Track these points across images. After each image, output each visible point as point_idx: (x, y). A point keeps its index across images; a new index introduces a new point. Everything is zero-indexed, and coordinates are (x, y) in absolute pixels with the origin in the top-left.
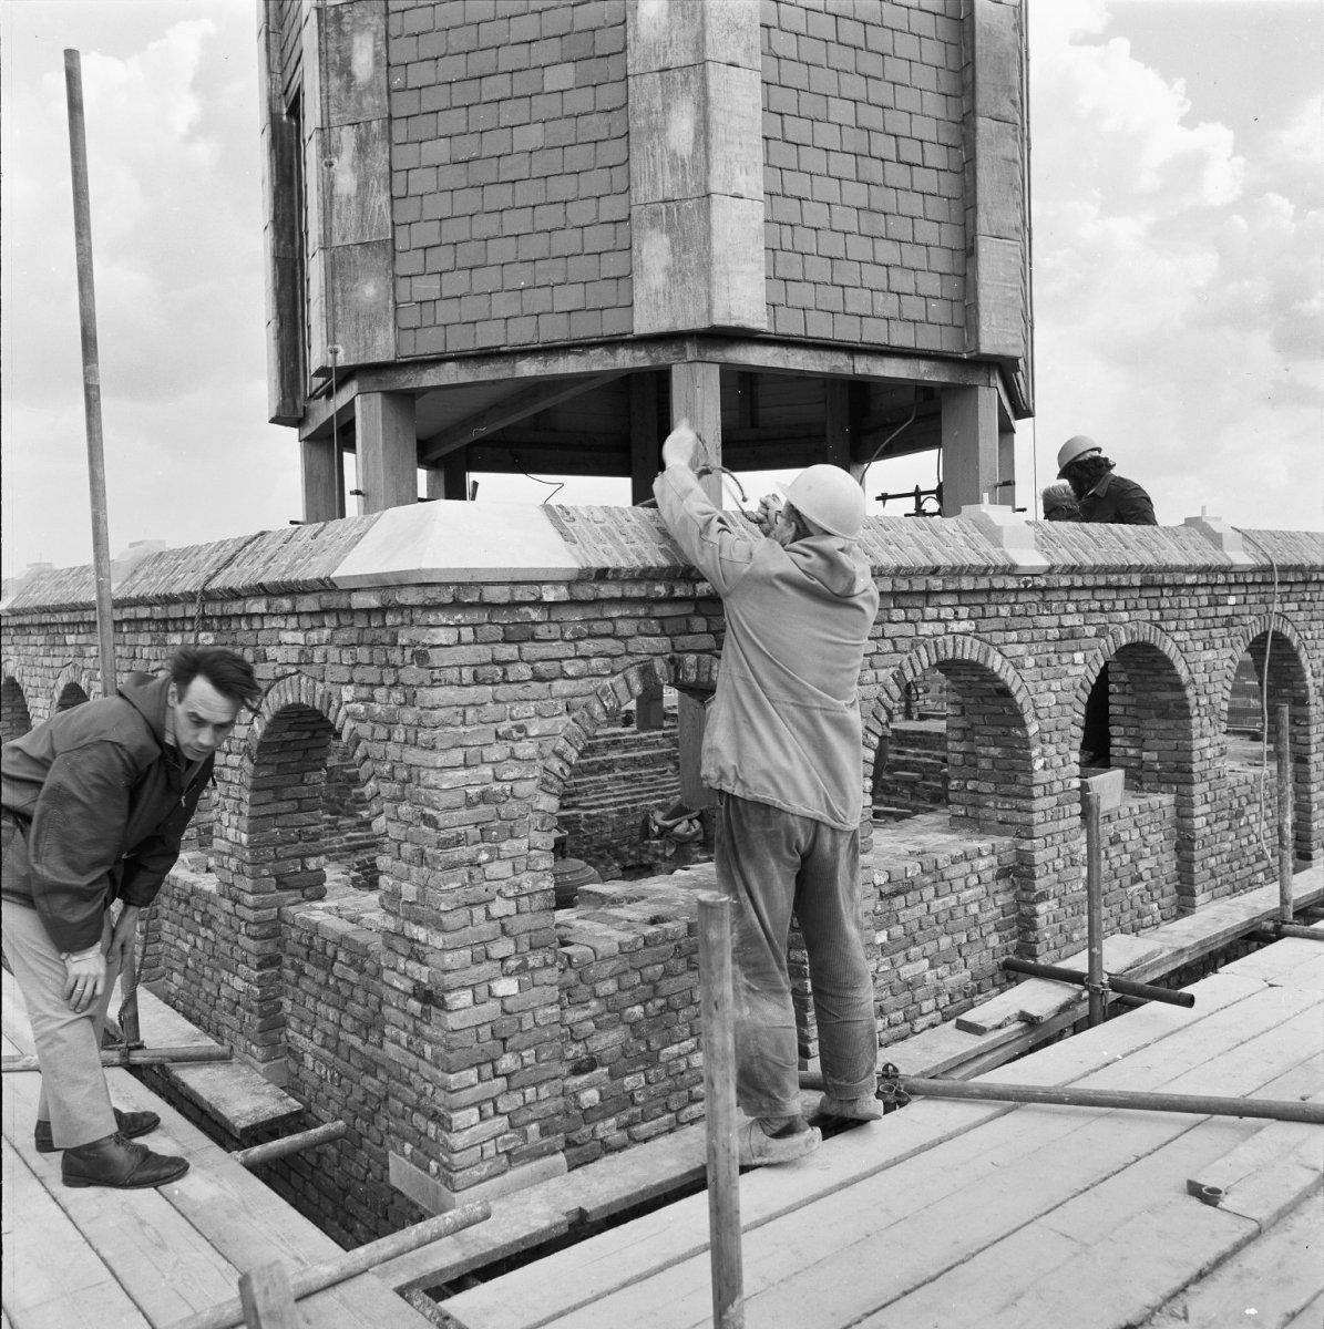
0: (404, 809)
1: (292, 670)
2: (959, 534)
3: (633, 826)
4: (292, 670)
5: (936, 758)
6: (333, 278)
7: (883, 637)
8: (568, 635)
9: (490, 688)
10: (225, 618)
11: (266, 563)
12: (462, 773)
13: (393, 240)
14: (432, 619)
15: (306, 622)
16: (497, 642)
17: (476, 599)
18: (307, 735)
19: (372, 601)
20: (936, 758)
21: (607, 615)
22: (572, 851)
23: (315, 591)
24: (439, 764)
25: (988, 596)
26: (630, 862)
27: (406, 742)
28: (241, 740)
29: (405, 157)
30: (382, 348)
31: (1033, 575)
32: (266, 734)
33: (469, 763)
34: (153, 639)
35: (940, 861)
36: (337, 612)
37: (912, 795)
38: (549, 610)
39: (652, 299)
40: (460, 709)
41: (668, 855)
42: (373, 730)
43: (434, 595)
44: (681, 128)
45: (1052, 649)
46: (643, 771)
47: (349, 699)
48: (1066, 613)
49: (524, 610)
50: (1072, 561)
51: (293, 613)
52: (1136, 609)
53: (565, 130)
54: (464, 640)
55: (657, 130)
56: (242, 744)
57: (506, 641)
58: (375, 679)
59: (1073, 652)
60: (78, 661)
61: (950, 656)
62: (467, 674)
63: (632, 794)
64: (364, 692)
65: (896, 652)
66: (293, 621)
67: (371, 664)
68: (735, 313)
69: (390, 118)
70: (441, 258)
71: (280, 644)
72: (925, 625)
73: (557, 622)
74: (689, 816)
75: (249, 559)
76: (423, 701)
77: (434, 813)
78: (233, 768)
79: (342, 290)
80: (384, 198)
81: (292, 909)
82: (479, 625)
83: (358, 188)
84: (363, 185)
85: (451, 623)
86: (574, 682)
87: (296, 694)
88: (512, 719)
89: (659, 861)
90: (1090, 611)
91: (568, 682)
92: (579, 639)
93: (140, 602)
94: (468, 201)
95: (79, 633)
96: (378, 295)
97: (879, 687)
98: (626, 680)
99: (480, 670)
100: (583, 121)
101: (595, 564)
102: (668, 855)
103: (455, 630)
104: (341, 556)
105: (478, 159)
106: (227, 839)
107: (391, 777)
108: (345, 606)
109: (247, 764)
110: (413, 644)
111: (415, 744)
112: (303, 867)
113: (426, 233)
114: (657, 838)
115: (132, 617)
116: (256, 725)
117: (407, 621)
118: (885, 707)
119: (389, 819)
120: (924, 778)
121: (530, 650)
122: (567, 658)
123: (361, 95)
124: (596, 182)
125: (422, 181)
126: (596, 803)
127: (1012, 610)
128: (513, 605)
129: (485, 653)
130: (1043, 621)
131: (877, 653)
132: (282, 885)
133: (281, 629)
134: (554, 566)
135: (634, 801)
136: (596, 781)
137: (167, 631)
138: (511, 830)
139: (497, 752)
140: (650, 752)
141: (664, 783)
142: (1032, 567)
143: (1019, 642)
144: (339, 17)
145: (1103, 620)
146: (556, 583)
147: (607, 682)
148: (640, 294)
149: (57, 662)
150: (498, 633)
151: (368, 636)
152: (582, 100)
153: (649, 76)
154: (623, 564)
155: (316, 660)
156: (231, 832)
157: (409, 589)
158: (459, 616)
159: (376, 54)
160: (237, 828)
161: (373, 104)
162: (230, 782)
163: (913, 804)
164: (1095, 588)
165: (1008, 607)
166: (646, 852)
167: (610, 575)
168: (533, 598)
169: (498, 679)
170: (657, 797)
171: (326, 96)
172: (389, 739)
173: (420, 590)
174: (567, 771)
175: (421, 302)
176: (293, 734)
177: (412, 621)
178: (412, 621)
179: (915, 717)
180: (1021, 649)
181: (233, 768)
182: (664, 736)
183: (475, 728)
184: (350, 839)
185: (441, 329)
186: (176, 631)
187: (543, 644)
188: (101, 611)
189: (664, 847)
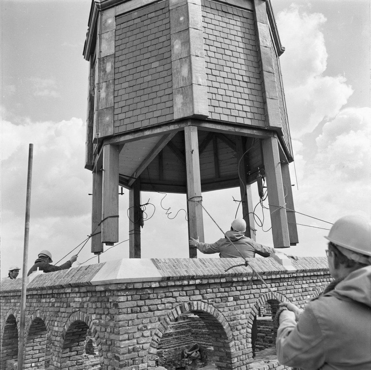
0: (109, 354)
1: (78, 310)
2: (270, 262)
3: (179, 354)
4: (78, 310)
5: (269, 329)
6: (99, 117)
7: (251, 294)
8: (159, 297)
9: (136, 314)
10: (59, 294)
11: (72, 277)
12: (127, 342)
13: (114, 106)
14: (119, 294)
15: (83, 295)
16: (138, 300)
17: (132, 287)
18: (81, 330)
19: (102, 289)
20: (269, 329)
21: (170, 290)
22: (160, 363)
23: (85, 286)
24: (120, 339)
25: (280, 280)
26: (178, 366)
27: (111, 332)
28: (61, 332)
29: (117, 87)
30: (110, 132)
31: (292, 273)
32: (68, 330)
33: (130, 338)
34: (37, 301)
35: (274, 365)
36: (92, 292)
37: (263, 341)
38: (153, 290)
39: (178, 111)
40: (127, 321)
41: (190, 363)
42: (101, 328)
43: (119, 287)
44: (185, 72)
45: (300, 295)
46: (181, 336)
47: (94, 318)
48: (303, 284)
49: (146, 290)
50: (303, 269)
51: (79, 292)
52: (323, 281)
53: (157, 76)
54: (128, 300)
55: (179, 72)
56: (61, 333)
57: (141, 300)
58: (102, 312)
59: (306, 295)
60: (14, 308)
61: (271, 298)
62: (129, 310)
63: (179, 343)
64: (98, 316)
65: (255, 298)
66: (78, 295)
67: (101, 308)
68: (200, 111)
69: (115, 79)
70: (126, 109)
71: (74, 302)
72: (263, 289)
73: (156, 293)
74: (196, 350)
75: (67, 276)
76: (116, 318)
77: (118, 355)
78: (58, 341)
79: (101, 120)
80: (112, 97)
82: (133, 295)
83: (106, 96)
84: (107, 95)
85: (125, 295)
86: (161, 311)
87: (78, 317)
88: (142, 323)
89: (187, 366)
90: (310, 283)
91: (159, 311)
92: (162, 298)
93: (35, 289)
94: (133, 95)
95: (15, 299)
96: (110, 119)
97: (251, 309)
98: (176, 310)
99: (133, 309)
100: (161, 73)
101: (166, 276)
102: (190, 363)
103: (126, 297)
104: (93, 276)
105: (135, 85)
106: (54, 365)
107: (106, 344)
108: (94, 290)
109: (62, 340)
110: (113, 301)
111: (114, 333)
113: (122, 104)
114: (187, 358)
115: (32, 294)
116: (66, 327)
117: (112, 294)
118: (253, 315)
119: (104, 358)
120: (266, 336)
121: (148, 302)
122: (159, 304)
123: (108, 75)
124: (164, 99)
125: (121, 92)
126: (167, 347)
127: (288, 284)
128: (143, 289)
129: (135, 303)
130: (297, 286)
131: (249, 299)
133: (75, 297)
134: (155, 277)
135: (179, 346)
136: (167, 340)
137: (41, 298)
138: (142, 360)
139: (138, 334)
140: (183, 330)
141: (188, 339)
142: (292, 271)
143: (291, 293)
144: (104, 60)
145: (314, 285)
146: (155, 282)
147: (170, 311)
148: (175, 109)
149: (8, 308)
150: (139, 297)
151: (100, 299)
152: (161, 69)
153: (177, 61)
154: (175, 275)
155: (85, 306)
156: (55, 363)
157: (113, 285)
158: (127, 293)
159: (112, 66)
160: (57, 362)
161: (111, 77)
162: (56, 346)
163: (264, 344)
164: (311, 276)
165: (286, 283)
166: (183, 363)
167: (171, 279)
168: (149, 286)
169: (138, 311)
170: (186, 344)
171: (99, 76)
172: (106, 331)
173: (116, 285)
174: (159, 340)
175: (120, 120)
176: (77, 329)
177: (113, 294)
178: (113, 294)
179: (262, 316)
180: (291, 295)
181: (58, 341)
182: (187, 324)
183: (131, 327)
184: (92, 362)
185: (125, 126)
186: (44, 298)
187: (152, 300)
188: (23, 293)
189: (189, 361)
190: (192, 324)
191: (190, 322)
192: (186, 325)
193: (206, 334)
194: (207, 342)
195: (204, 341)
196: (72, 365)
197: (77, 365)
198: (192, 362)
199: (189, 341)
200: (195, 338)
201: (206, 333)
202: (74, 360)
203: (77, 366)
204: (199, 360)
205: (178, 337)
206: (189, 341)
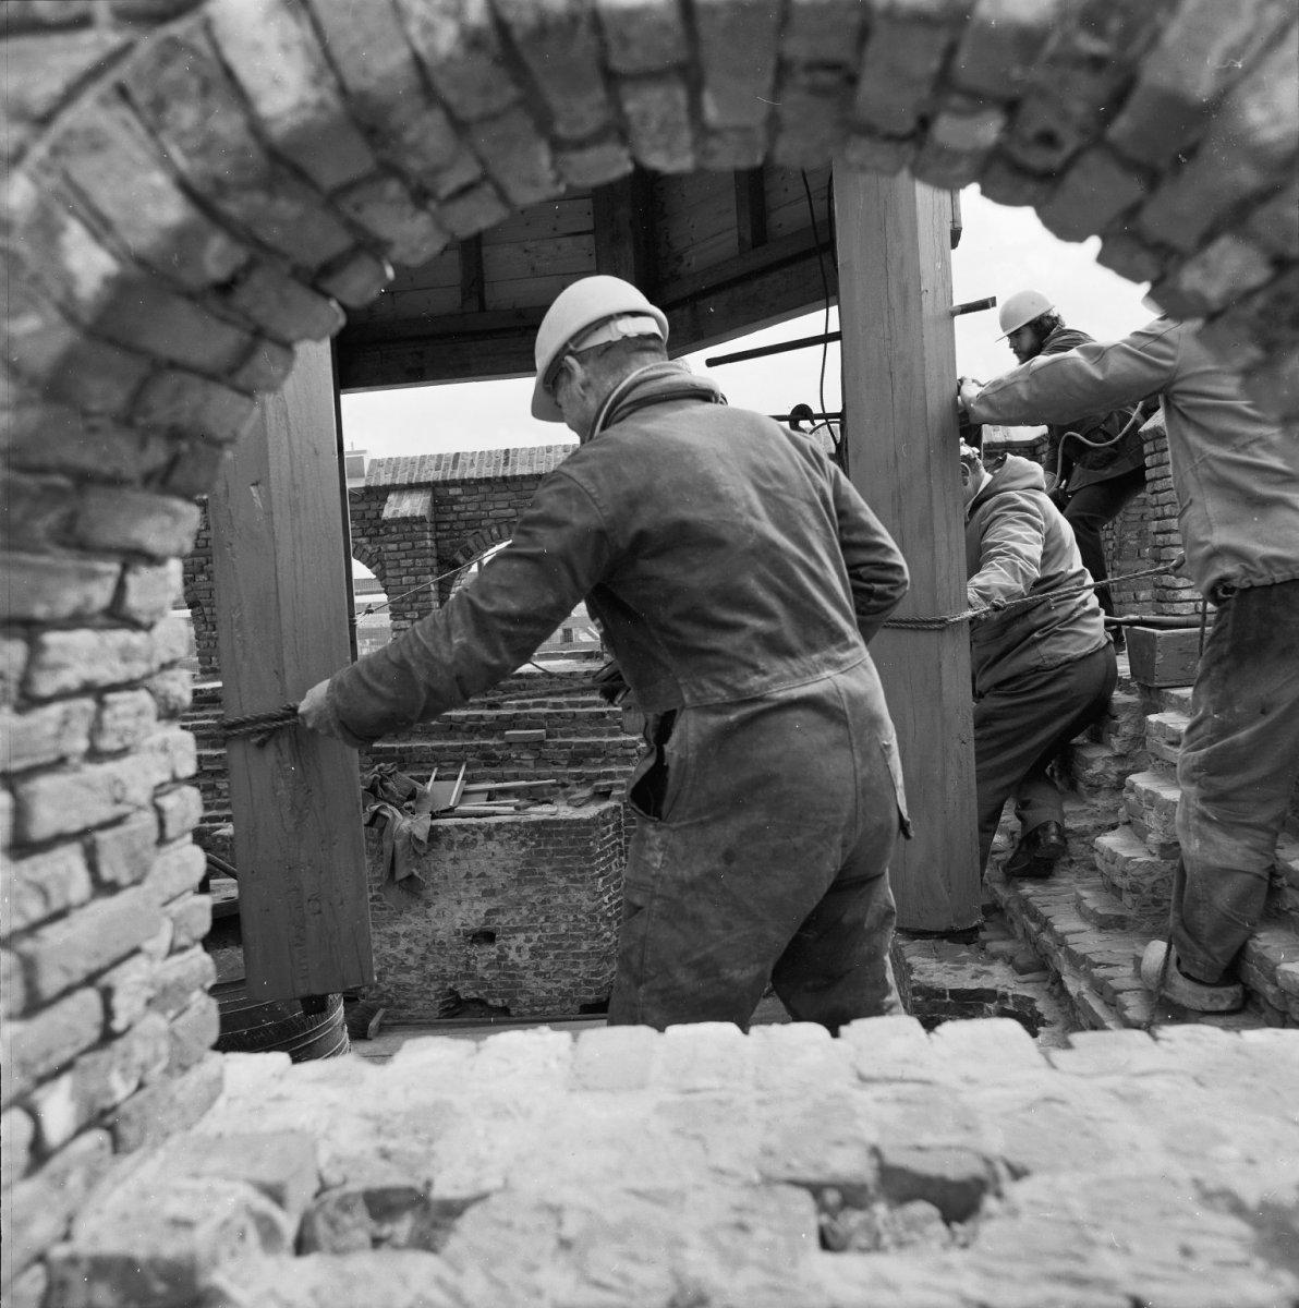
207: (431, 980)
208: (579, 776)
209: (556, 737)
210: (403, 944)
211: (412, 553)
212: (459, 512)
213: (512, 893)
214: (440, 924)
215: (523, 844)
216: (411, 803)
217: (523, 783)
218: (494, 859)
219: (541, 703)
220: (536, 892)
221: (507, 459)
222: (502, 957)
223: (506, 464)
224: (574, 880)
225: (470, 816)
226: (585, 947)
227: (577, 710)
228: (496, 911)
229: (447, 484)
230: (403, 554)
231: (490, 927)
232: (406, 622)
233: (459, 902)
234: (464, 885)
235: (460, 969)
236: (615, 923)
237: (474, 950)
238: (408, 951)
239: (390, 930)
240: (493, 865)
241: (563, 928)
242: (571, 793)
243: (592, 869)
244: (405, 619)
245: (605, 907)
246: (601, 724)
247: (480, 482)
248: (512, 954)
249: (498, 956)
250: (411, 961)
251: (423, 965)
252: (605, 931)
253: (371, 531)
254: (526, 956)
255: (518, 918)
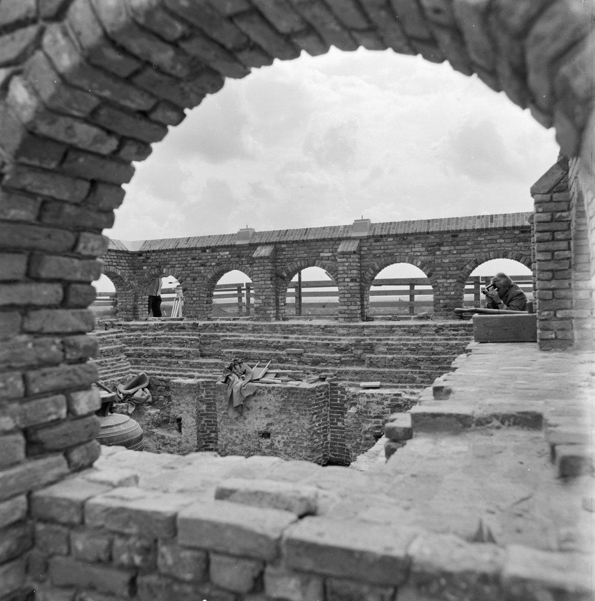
41: (130, 412)
46: (107, 359)
81: (61, 491)
102: (130, 412)
112: (70, 411)
120: (305, 352)
132: (35, 447)
141: (120, 366)
163: (300, 367)
170: (118, 375)
179: (281, 319)
182: (117, 337)
190: (126, 337)
191: (121, 334)
192: (114, 339)
193: (162, 355)
194: (165, 370)
195: (158, 369)
196: (44, 356)
197: (65, 360)
198: (134, 409)
199: (122, 370)
200: (135, 364)
201: (163, 352)
202: (48, 329)
203: (64, 367)
204: (148, 405)
205: (102, 362)
206: (122, 370)
207: (245, 450)
208: (314, 370)
209: (308, 353)
210: (235, 433)
211: (263, 272)
212: (286, 255)
213: (277, 417)
214: (248, 427)
215: (282, 397)
216: (244, 375)
217: (291, 371)
218: (270, 402)
219: (306, 337)
220: (287, 418)
221: (306, 233)
222: (272, 444)
223: (305, 235)
224: (302, 415)
225: (264, 383)
226: (305, 444)
227: (318, 342)
228: (271, 424)
229: (280, 243)
230: (260, 272)
231: (269, 431)
232: (260, 300)
233: (257, 419)
234: (259, 412)
235: (256, 447)
236: (322, 436)
237: (263, 440)
238: (237, 437)
239: (230, 427)
240: (270, 404)
241: (297, 435)
242: (310, 377)
243: (310, 410)
244: (260, 299)
245: (316, 428)
246: (327, 348)
247: (293, 242)
248: (276, 444)
249: (271, 444)
250: (237, 441)
251: (241, 444)
252: (316, 438)
253: (251, 262)
254: (282, 445)
255: (279, 428)
